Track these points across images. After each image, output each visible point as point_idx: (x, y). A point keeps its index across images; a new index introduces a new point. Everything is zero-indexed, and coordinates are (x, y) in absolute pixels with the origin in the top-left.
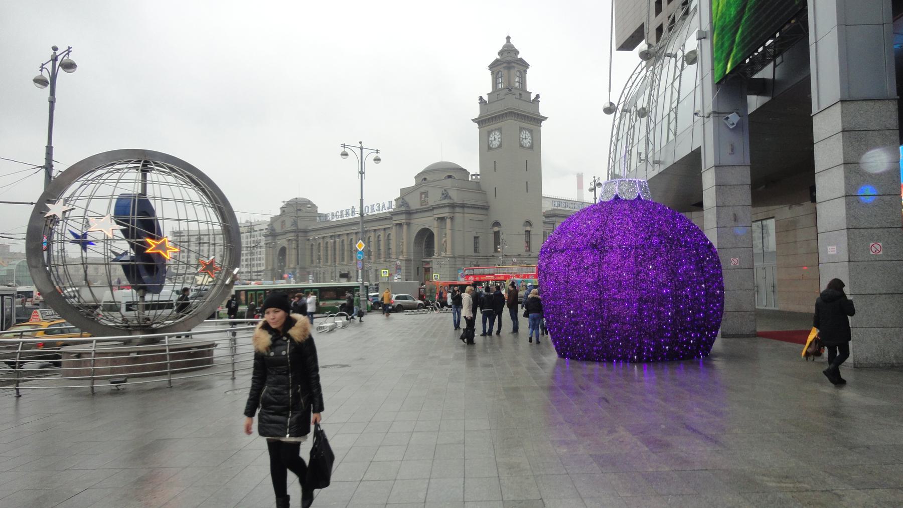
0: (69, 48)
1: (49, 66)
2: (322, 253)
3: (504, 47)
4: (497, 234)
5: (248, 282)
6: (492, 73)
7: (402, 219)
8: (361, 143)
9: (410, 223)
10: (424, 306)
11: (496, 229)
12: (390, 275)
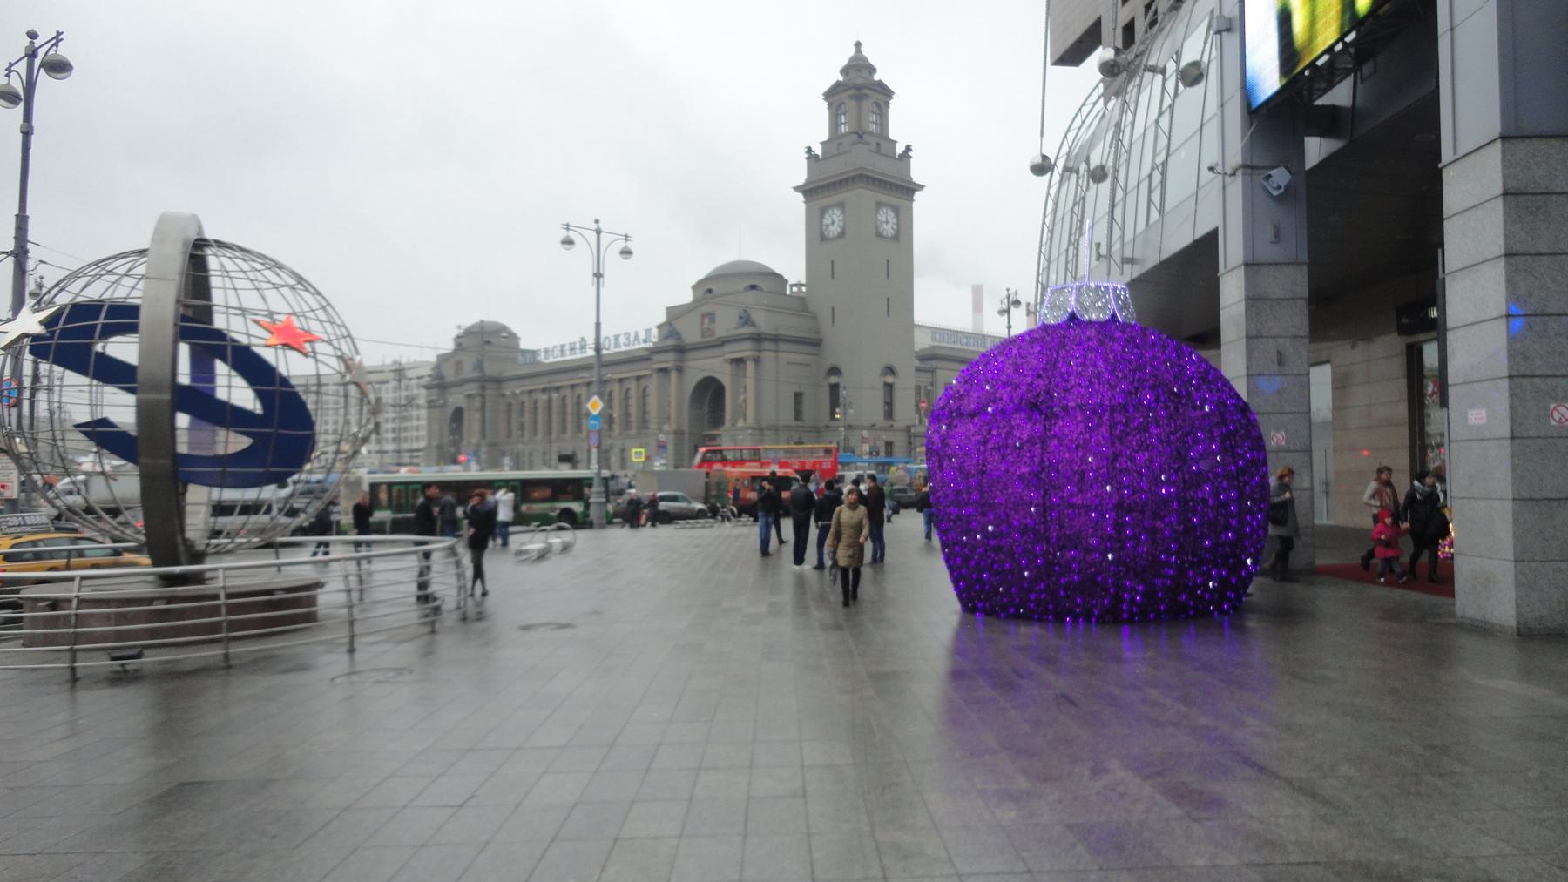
0: (59, 34)
1: (22, 67)
2: (527, 418)
3: (852, 60)
4: (834, 389)
5: (395, 468)
6: (830, 105)
7: (668, 360)
8: (597, 221)
9: (681, 367)
10: (713, 512)
11: (833, 380)
12: (648, 458)
